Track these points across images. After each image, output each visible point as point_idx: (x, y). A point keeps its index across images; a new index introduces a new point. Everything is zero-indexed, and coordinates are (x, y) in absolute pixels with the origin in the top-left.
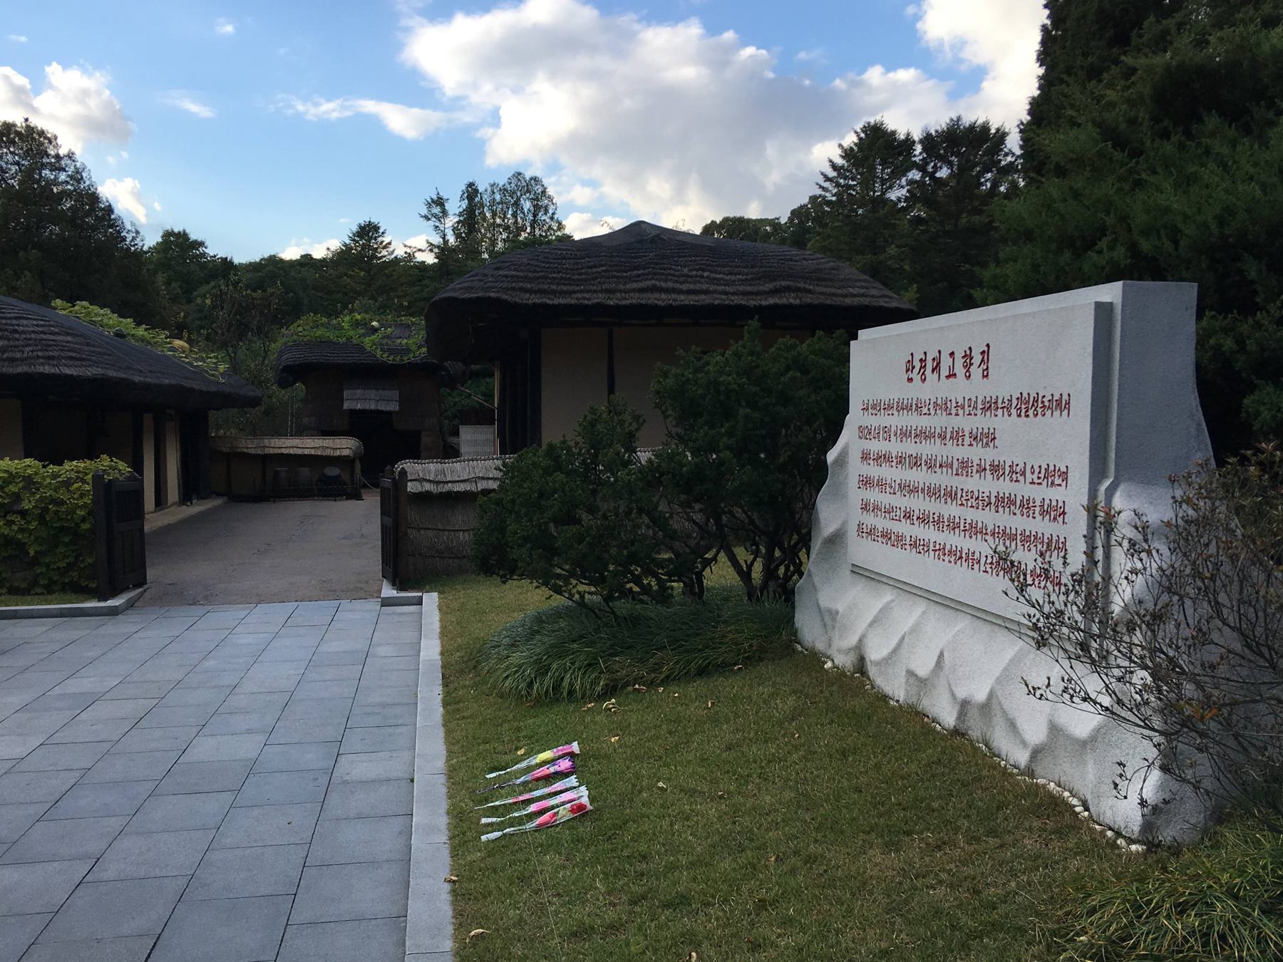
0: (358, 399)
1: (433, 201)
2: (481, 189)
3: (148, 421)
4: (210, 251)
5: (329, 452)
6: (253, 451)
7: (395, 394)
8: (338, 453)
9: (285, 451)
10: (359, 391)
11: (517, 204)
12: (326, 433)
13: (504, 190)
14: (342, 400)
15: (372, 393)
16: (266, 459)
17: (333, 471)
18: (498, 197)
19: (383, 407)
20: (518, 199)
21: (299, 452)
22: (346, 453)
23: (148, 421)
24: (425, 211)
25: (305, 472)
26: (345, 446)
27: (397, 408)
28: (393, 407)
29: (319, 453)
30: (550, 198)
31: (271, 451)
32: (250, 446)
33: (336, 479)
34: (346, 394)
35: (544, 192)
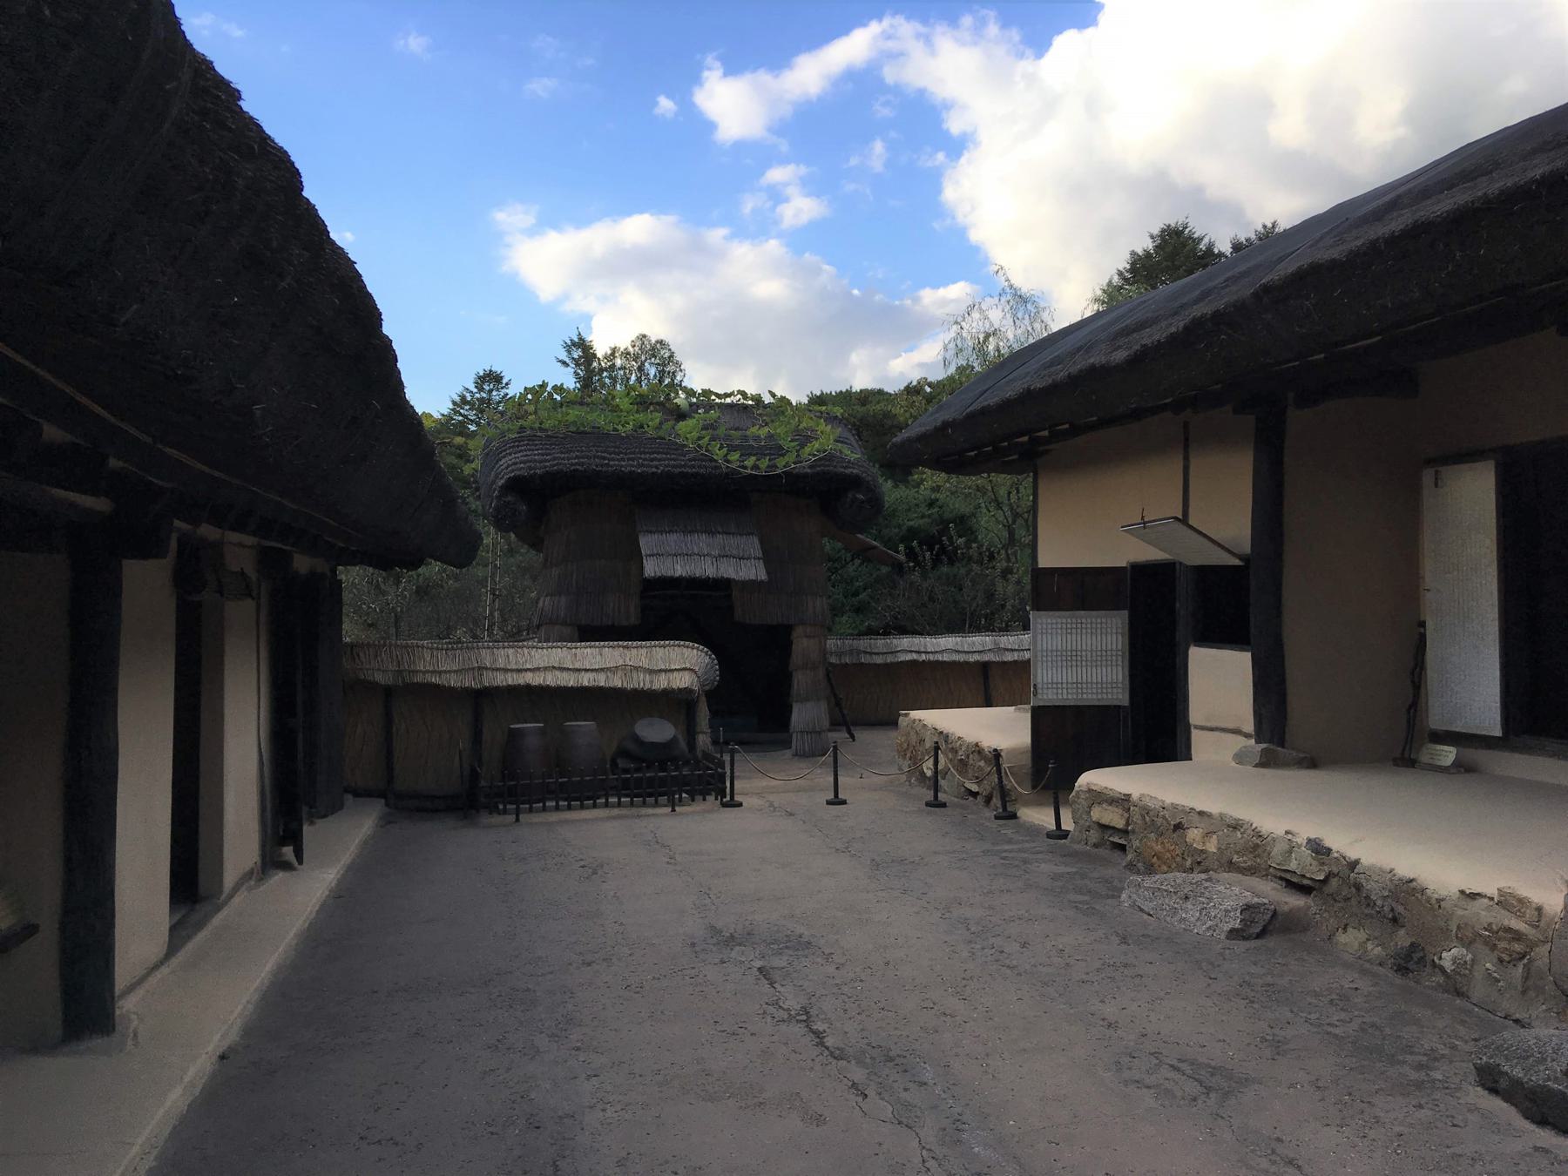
0: (672, 555)
1: (574, 344)
2: (600, 354)
3: (146, 587)
4: (241, 103)
5: (642, 682)
6: (454, 681)
7: (753, 545)
8: (661, 683)
9: (535, 680)
10: (673, 537)
11: (641, 369)
12: (590, 633)
13: (626, 354)
14: (636, 556)
15: (701, 542)
16: (482, 699)
17: (657, 731)
18: (618, 362)
19: (729, 570)
20: (643, 364)
21: (569, 680)
22: (682, 681)
23: (146, 587)
24: (564, 356)
25: (584, 729)
26: (678, 664)
27: (763, 575)
28: (753, 571)
29: (617, 682)
30: (678, 364)
31: (501, 680)
32: (444, 666)
33: (662, 755)
34: (646, 543)
35: (671, 356)
